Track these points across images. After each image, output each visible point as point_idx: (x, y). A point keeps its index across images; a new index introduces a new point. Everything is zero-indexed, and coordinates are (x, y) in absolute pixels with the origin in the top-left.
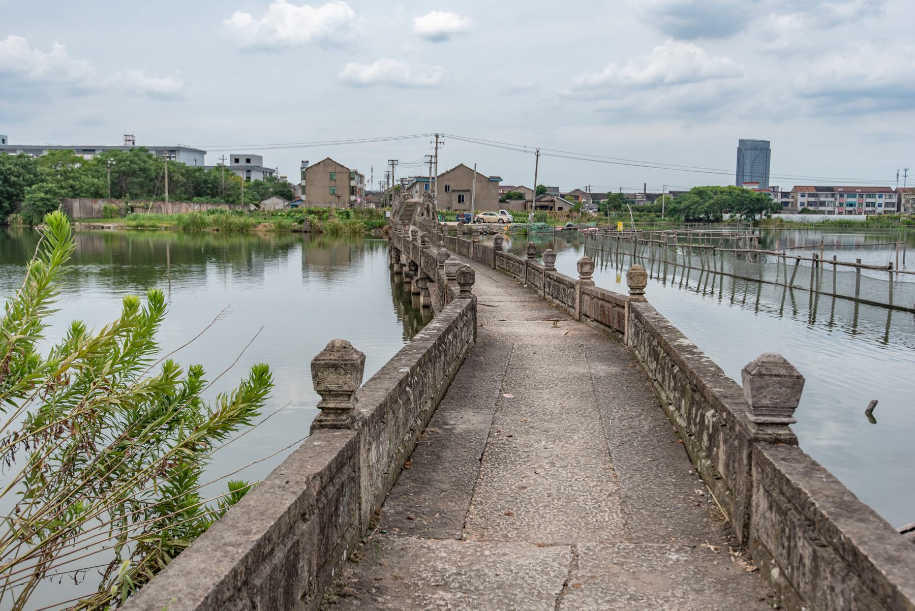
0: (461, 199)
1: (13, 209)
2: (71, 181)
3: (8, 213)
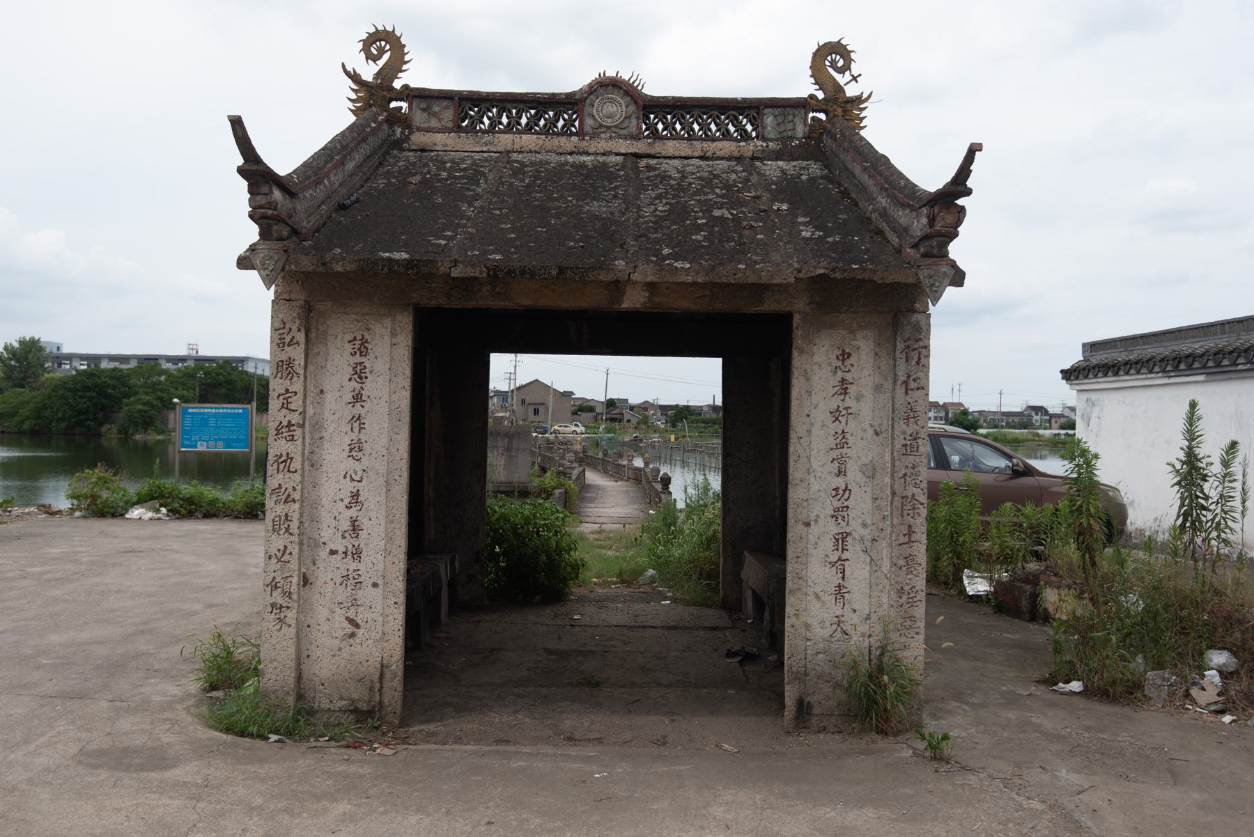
0: (536, 412)
1: (107, 419)
2: (160, 393)
3: (101, 424)
